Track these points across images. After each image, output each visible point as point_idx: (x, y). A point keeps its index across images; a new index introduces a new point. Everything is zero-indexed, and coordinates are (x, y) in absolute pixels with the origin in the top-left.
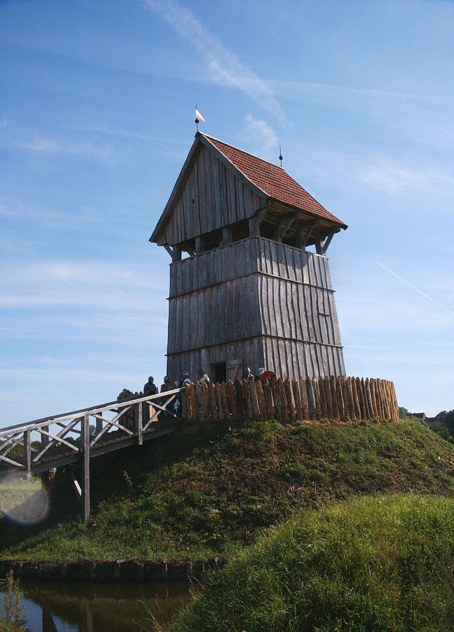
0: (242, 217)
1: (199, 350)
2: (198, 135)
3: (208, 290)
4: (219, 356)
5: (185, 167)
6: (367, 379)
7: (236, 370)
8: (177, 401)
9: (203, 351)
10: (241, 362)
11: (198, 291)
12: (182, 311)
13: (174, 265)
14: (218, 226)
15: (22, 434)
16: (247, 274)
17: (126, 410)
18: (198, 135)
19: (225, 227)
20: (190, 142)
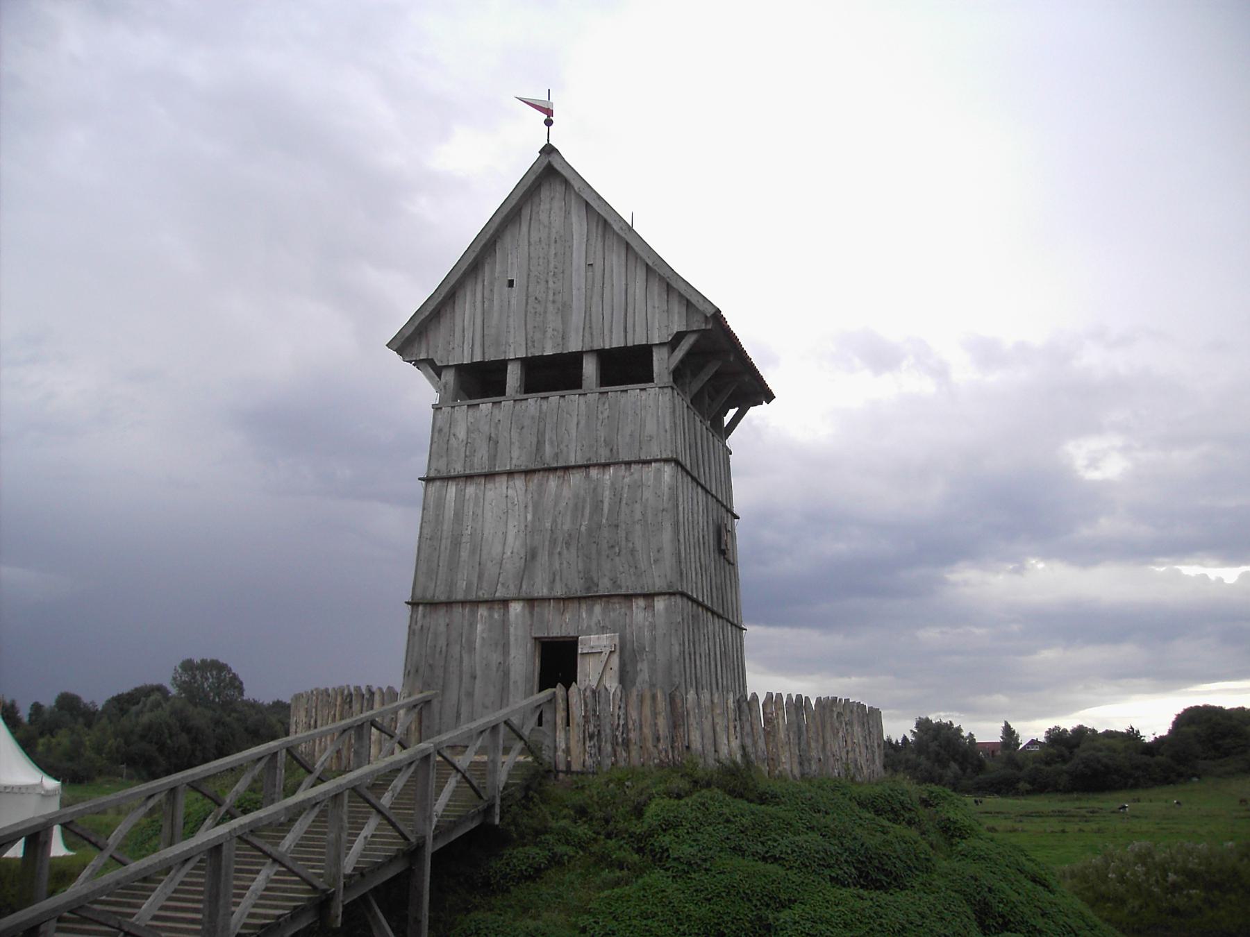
0: (640, 340)
1: (505, 602)
2: (548, 150)
3: (536, 478)
4: (558, 625)
5: (505, 211)
6: (789, 696)
7: (604, 657)
8: (21, 844)
9: (516, 608)
10: (617, 641)
11: (510, 474)
12: (458, 516)
13: (446, 410)
14: (574, 346)
15: (162, 796)
16: (643, 457)
17: (399, 782)
18: (548, 150)
19: (592, 351)
20: (525, 159)
